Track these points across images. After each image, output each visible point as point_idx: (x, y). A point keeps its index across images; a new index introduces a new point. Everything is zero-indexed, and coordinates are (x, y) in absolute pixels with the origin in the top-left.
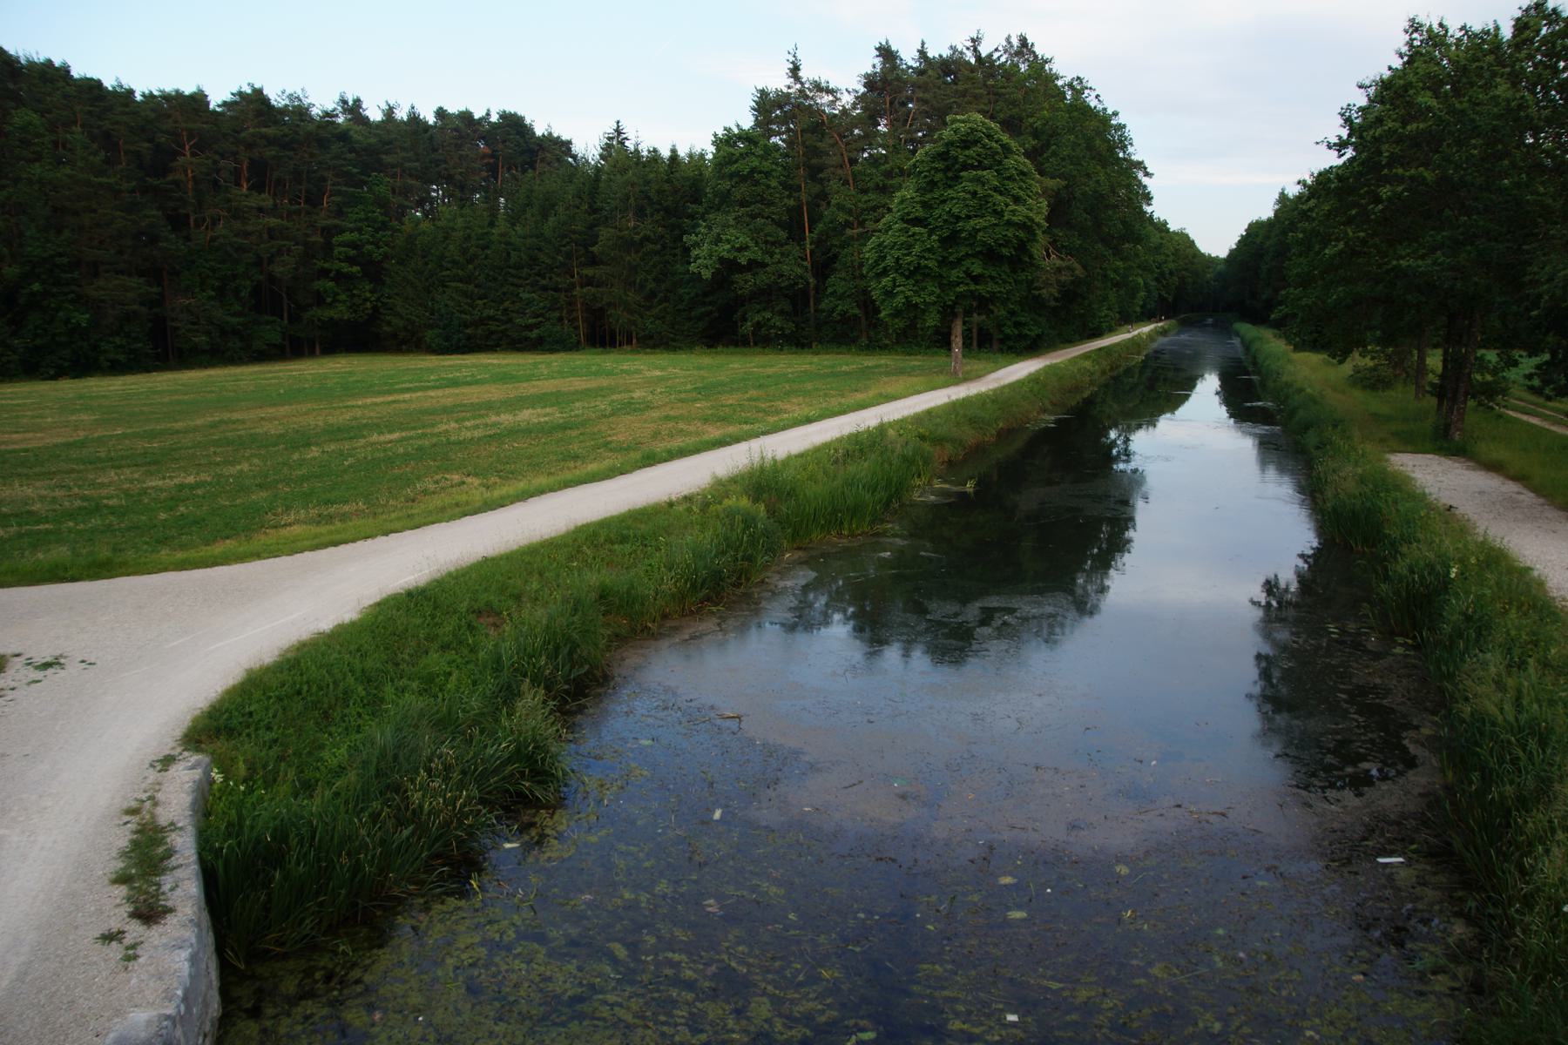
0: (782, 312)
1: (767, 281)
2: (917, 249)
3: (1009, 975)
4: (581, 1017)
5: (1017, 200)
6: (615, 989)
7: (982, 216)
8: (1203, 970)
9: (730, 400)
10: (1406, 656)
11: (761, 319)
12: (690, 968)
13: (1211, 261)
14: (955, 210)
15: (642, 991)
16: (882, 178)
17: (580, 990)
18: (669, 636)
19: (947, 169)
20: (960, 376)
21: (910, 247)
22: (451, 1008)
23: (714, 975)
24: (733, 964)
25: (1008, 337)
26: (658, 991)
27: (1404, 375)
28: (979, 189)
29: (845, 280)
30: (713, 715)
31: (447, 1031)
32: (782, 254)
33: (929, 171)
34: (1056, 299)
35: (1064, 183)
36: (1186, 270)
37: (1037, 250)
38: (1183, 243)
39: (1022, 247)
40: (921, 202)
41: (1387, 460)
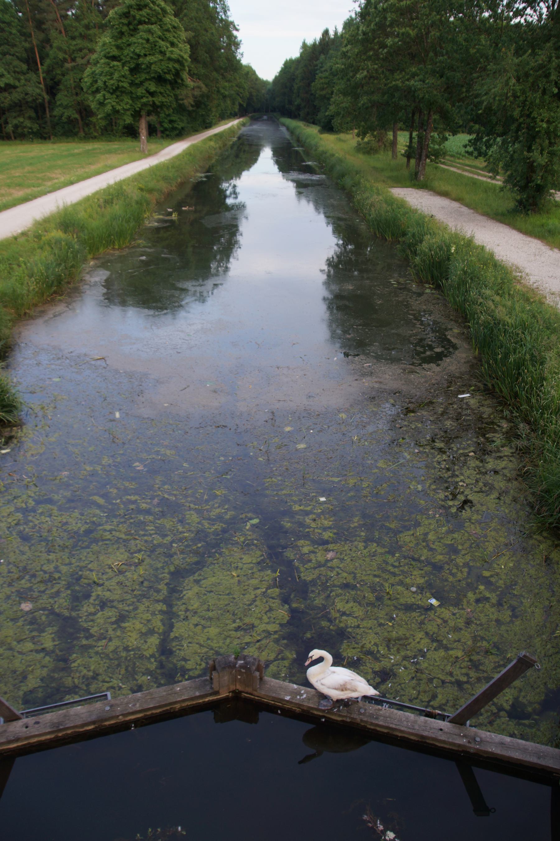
0: (30, 118)
1: (18, 97)
2: (116, 76)
3: (311, 478)
4: (96, 541)
5: (173, 44)
6: (107, 522)
7: (153, 55)
8: (402, 461)
9: (17, 173)
10: (433, 294)
11: (17, 122)
12: (143, 503)
13: (265, 83)
14: (137, 51)
15: (122, 520)
16: (83, 29)
17: (87, 526)
18: (40, 316)
19: (129, 24)
20: (146, 152)
21: (112, 74)
22: (17, 552)
23: (158, 504)
24: (166, 496)
25: (166, 129)
26: (132, 518)
27: (383, 146)
28: (151, 38)
29: (66, 96)
30: (88, 359)
31: (21, 565)
32: (26, 80)
33: (119, 25)
34: (192, 106)
35: (193, 34)
36: (253, 88)
37: (185, 75)
38: (249, 73)
39: (177, 74)
40: (115, 45)
41: (390, 192)
